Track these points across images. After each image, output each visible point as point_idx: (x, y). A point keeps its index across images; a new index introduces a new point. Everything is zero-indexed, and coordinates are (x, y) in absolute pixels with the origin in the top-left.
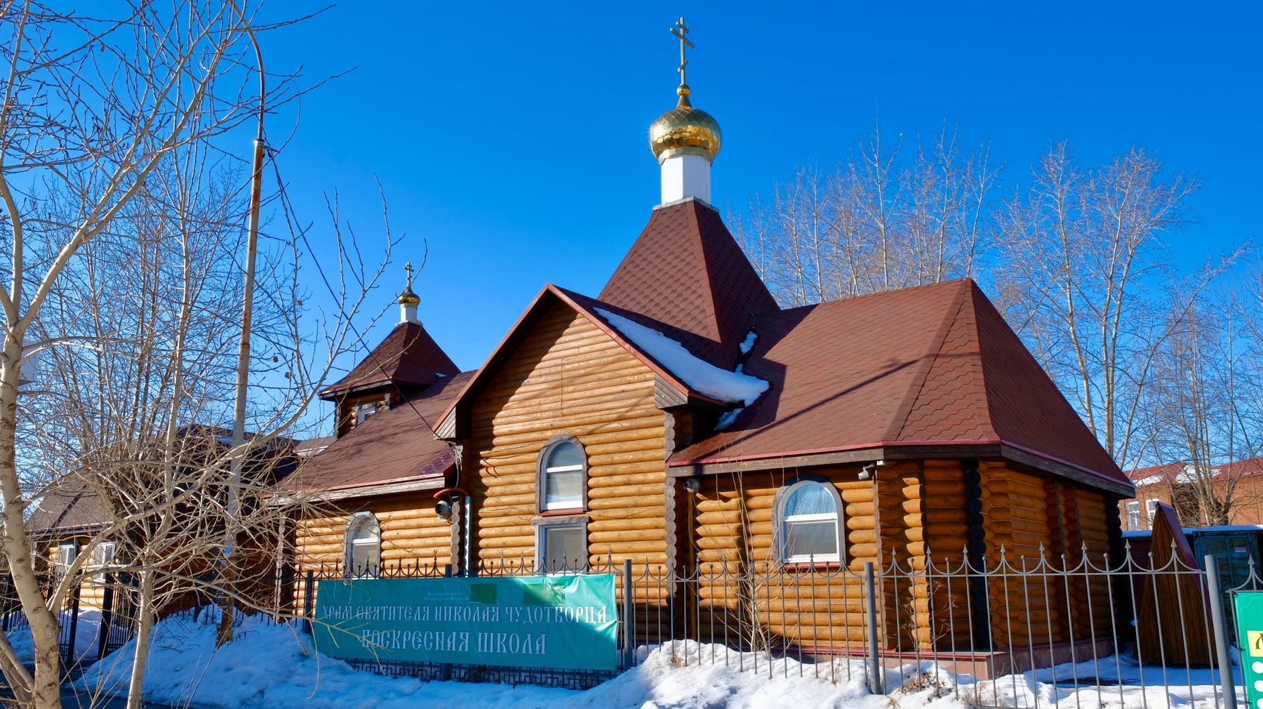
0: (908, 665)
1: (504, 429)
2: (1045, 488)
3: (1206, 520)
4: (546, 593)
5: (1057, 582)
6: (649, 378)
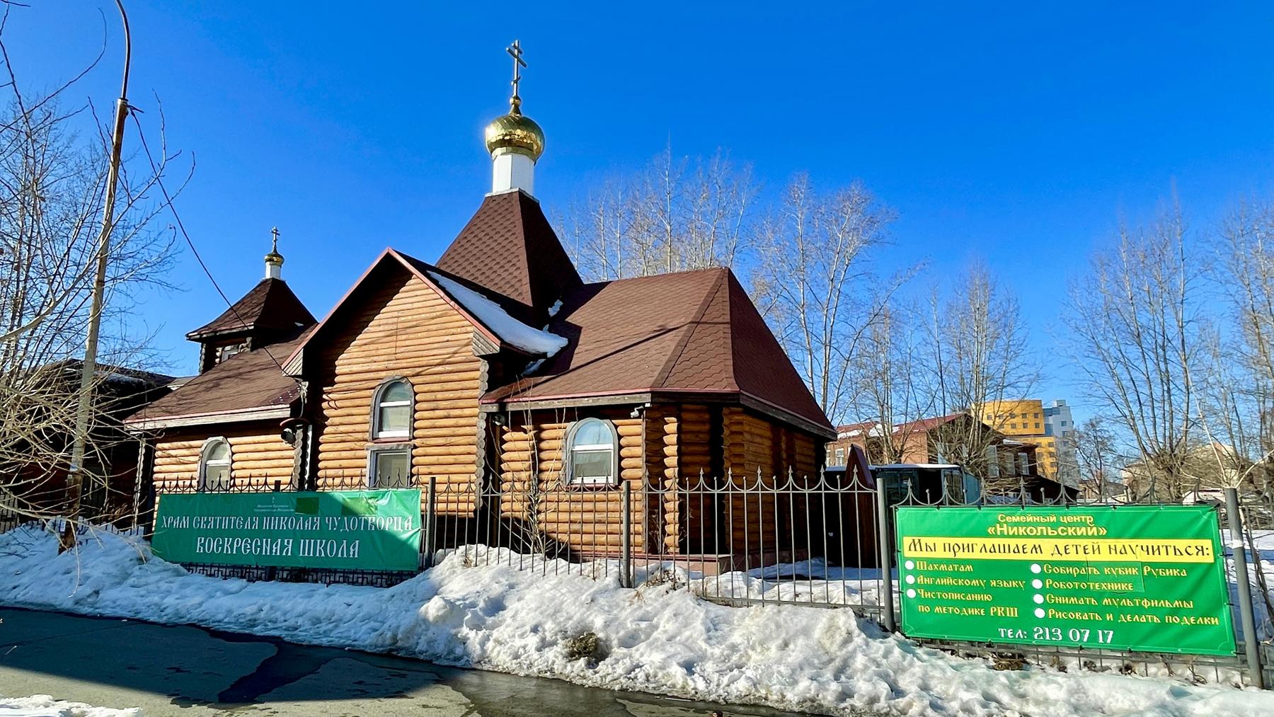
0: (653, 564)
1: (346, 369)
2: (772, 431)
3: (887, 462)
4: (360, 507)
5: (799, 498)
6: (471, 329)
